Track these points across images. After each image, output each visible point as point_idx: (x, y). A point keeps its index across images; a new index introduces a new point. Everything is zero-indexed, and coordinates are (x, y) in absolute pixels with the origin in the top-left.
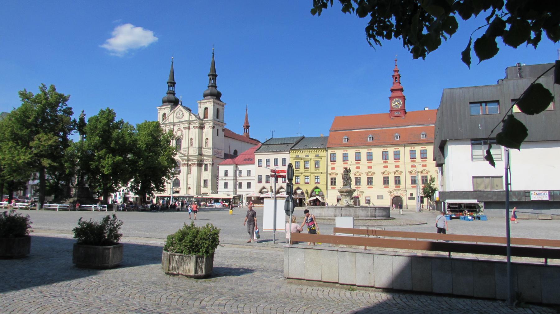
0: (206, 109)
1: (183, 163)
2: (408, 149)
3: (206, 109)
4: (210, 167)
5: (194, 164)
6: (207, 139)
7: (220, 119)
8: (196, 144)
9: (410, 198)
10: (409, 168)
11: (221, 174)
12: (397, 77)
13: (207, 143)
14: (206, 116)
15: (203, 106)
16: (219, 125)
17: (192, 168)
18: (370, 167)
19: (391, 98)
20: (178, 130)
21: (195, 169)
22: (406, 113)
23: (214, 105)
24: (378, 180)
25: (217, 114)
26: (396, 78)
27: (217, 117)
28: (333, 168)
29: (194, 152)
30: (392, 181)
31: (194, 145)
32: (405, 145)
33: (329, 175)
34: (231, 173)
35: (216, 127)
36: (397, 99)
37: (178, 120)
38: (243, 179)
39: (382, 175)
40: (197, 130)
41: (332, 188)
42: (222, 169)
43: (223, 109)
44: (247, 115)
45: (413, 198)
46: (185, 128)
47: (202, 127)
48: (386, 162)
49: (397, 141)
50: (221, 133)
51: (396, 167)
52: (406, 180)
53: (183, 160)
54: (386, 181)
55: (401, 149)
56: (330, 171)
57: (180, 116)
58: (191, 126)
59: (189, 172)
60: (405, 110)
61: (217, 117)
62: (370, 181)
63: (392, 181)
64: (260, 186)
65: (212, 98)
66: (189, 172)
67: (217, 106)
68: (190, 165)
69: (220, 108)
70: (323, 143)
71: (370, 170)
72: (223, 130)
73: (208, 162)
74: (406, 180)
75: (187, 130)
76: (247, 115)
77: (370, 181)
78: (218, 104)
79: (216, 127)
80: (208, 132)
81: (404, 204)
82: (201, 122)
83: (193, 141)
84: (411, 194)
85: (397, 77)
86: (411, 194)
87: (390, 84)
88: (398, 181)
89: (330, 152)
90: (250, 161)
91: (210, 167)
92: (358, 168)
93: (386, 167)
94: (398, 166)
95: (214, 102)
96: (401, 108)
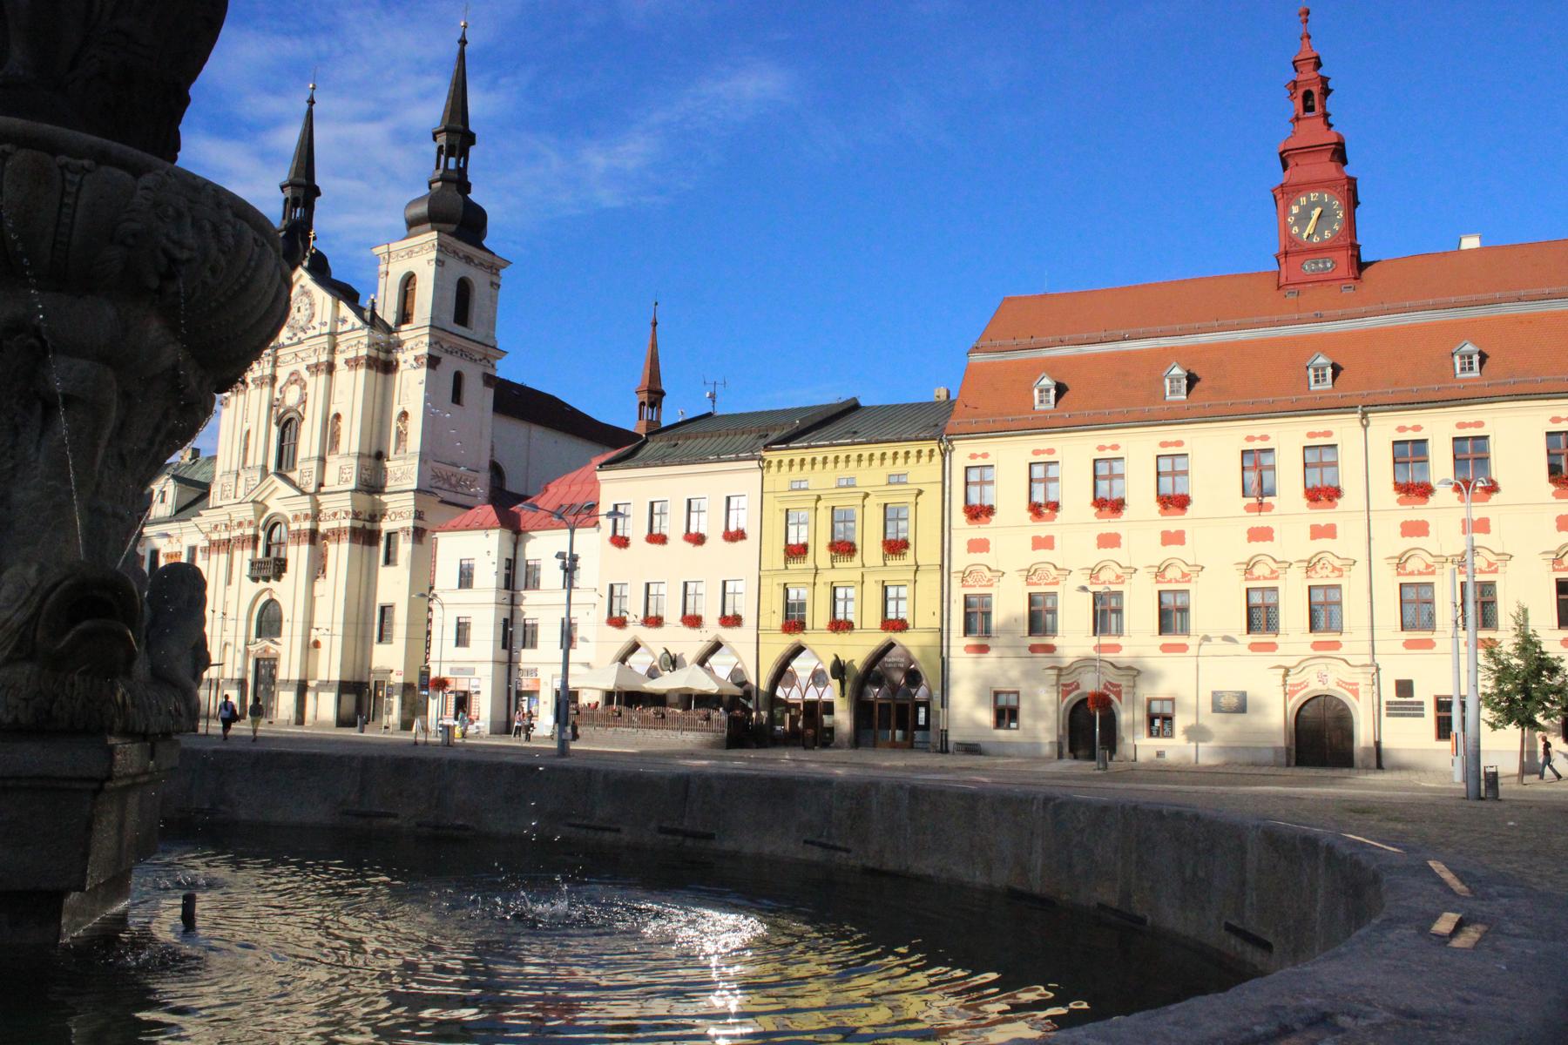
0: (409, 281)
1: (294, 527)
2: (1387, 427)
3: (409, 281)
4: (404, 547)
5: (336, 534)
6: (404, 415)
7: (476, 330)
8: (351, 438)
9: (1395, 710)
10: (1390, 541)
11: (446, 576)
12: (1312, 98)
13: (401, 436)
14: (405, 316)
15: (397, 270)
16: (463, 353)
17: (332, 548)
18: (1173, 538)
19: (1285, 193)
20: (290, 382)
21: (339, 554)
22: (1361, 266)
23: (439, 263)
25: (461, 303)
26: (1308, 95)
27: (462, 316)
28: (979, 546)
29: (343, 471)
30: (1293, 613)
31: (343, 446)
32: (1366, 407)
33: (956, 582)
34: (488, 576)
35: (450, 364)
36: (1313, 196)
38: (542, 607)
39: (1239, 575)
40: (362, 372)
42: (452, 547)
43: (495, 285)
44: (654, 346)
45: (1416, 710)
46: (314, 369)
47: (383, 365)
48: (1260, 507)
49: (1322, 395)
50: (479, 397)
51: (1318, 532)
52: (1369, 607)
53: (296, 518)
54: (1261, 617)
55: (1343, 429)
56: (961, 558)
58: (339, 360)
59: (318, 568)
60: (1356, 248)
61: (462, 316)
62: (1171, 617)
63: (1293, 613)
64: (622, 638)
65: (433, 229)
66: (318, 568)
67: (458, 269)
68: (325, 537)
69: (479, 278)
70: (931, 423)
71: (1173, 550)
72: (490, 380)
73: (399, 511)
74: (1369, 607)
75: (322, 377)
76: (654, 346)
77: (1171, 617)
78: (468, 259)
79: (450, 364)
80: (411, 387)
81: (1363, 736)
82: (381, 336)
83: (344, 425)
84: (1404, 688)
85: (1312, 98)
86: (1404, 688)
87: (1278, 123)
88: (1323, 613)
89: (963, 452)
90: (581, 514)
91: (404, 547)
92: (1109, 541)
93: (1261, 535)
94: (1328, 532)
95: (442, 248)
96: (1337, 236)
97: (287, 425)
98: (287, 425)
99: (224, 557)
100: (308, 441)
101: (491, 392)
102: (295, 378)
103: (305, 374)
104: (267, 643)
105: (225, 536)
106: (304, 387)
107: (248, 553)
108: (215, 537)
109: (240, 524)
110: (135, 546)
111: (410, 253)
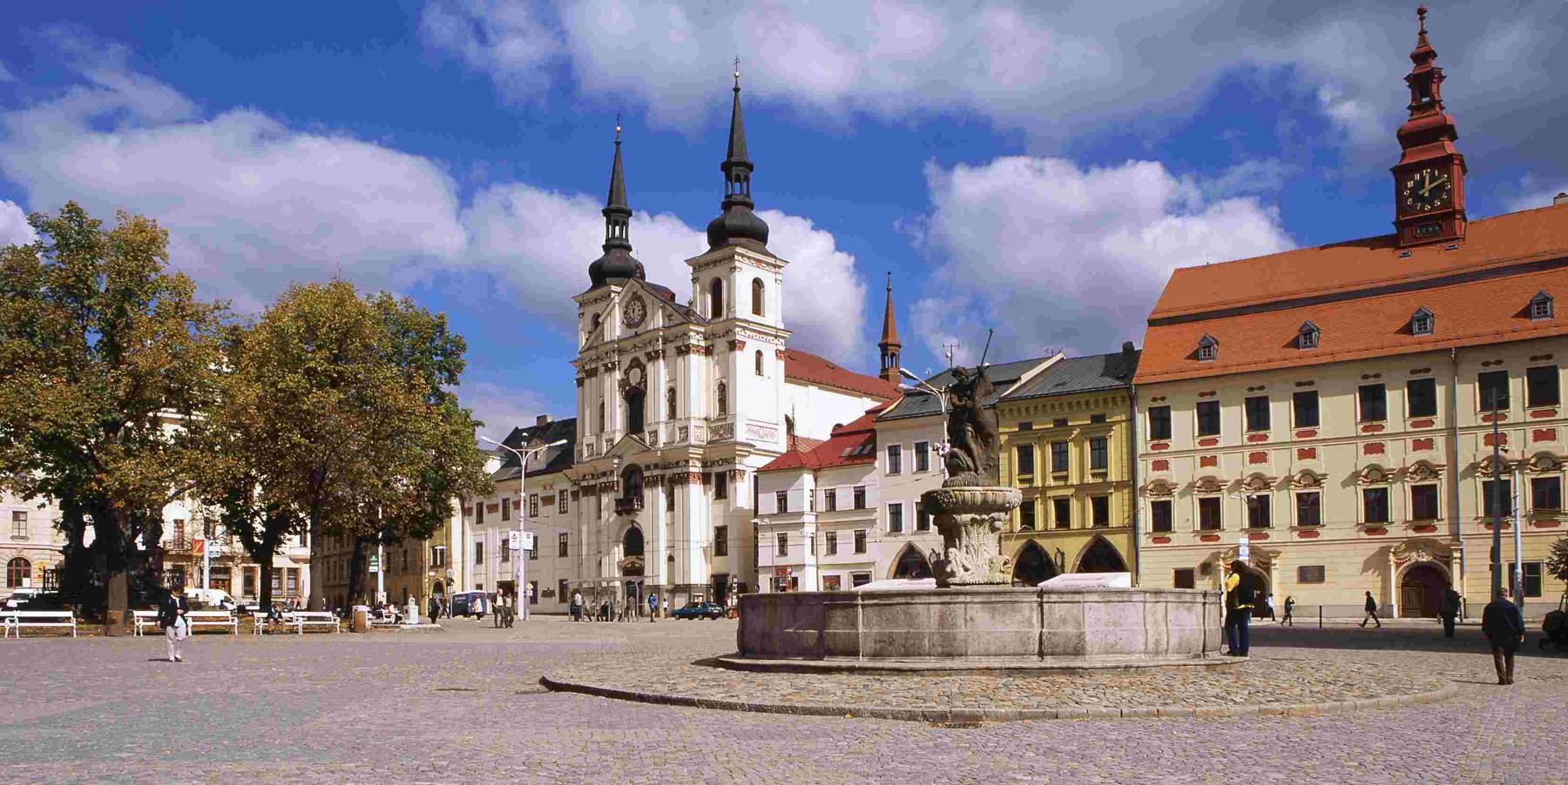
17: (678, 491)
20: (631, 367)
24: (1342, 507)
30: (1400, 503)
37: (632, 332)
41: (1156, 540)
56: (1146, 474)
57: (636, 315)
62: (1309, 512)
63: (1400, 503)
64: (897, 545)
69: (767, 277)
77: (1309, 512)
97: (635, 398)
98: (635, 398)
99: (593, 499)
100: (657, 408)
101: (782, 363)
102: (636, 363)
103: (643, 360)
104: (633, 558)
105: (592, 482)
106: (643, 369)
107: (612, 495)
108: (584, 484)
109: (604, 474)
110: (882, 430)
111: (715, 263)
